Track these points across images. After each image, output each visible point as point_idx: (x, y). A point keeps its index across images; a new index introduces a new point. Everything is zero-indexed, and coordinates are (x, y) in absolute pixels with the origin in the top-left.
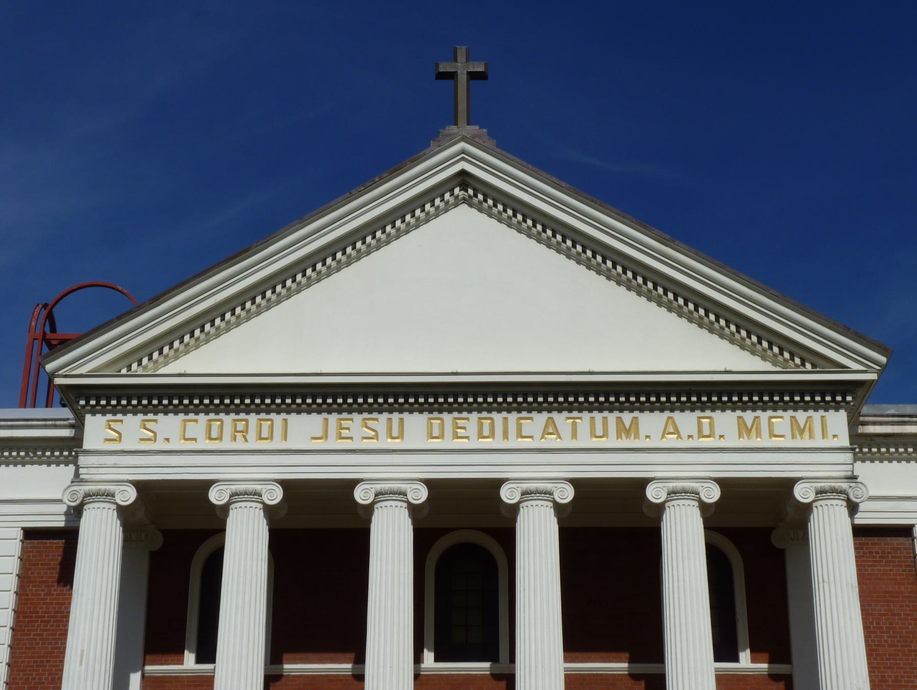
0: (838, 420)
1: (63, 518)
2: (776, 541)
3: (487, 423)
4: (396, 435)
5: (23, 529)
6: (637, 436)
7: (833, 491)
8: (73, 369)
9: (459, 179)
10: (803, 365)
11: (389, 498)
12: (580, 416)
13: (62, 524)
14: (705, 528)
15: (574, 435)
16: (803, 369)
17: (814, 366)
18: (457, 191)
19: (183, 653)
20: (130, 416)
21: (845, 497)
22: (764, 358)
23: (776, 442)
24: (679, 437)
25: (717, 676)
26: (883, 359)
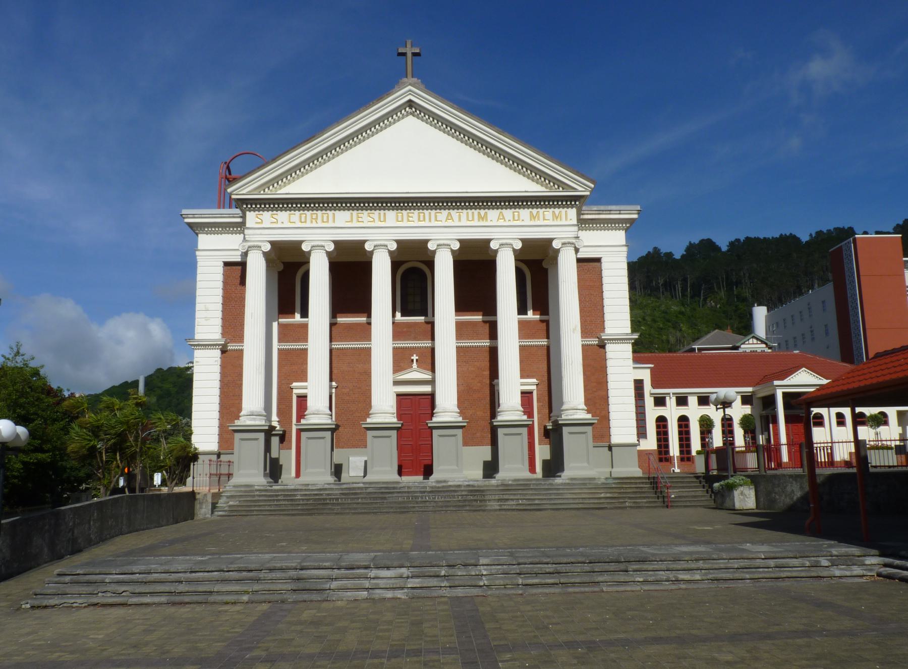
0: (572, 213)
1: (240, 257)
2: (545, 265)
3: (325, 216)
5: (223, 262)
7: (569, 243)
8: (240, 191)
9: (408, 104)
10: (559, 188)
13: (240, 260)
14: (515, 260)
15: (460, 220)
16: (558, 190)
17: (563, 189)
18: (407, 109)
19: (295, 314)
20: (266, 212)
22: (542, 185)
23: (546, 223)
24: (505, 220)
25: (518, 321)
26: (592, 186)
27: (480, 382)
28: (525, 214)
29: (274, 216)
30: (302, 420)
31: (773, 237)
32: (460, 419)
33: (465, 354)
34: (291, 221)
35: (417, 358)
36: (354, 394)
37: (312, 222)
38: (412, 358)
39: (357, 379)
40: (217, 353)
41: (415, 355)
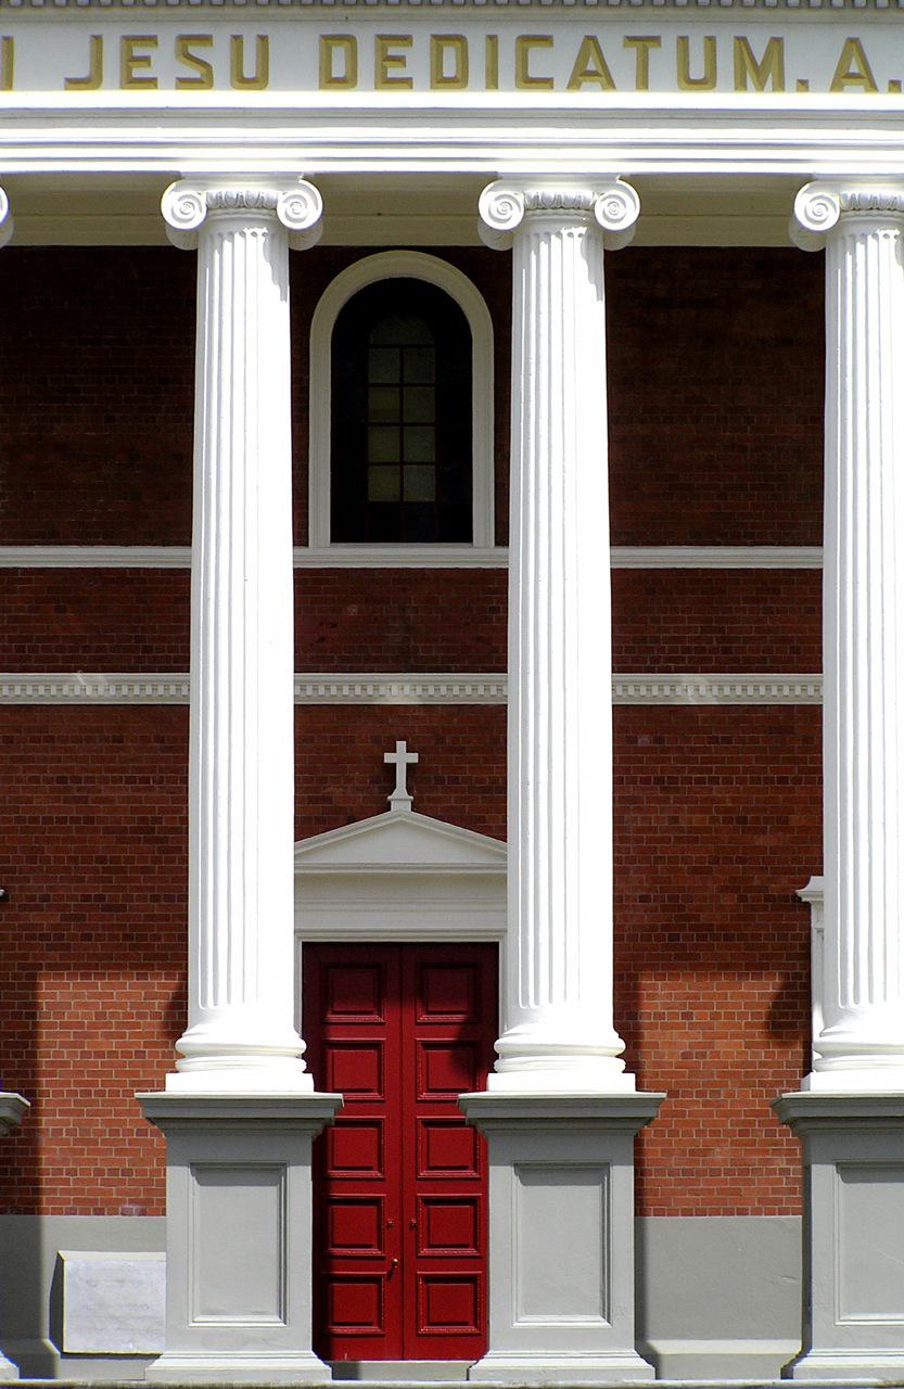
4: (701, 76)
6: (780, 86)
11: (870, 218)
12: (656, 34)
21: (214, 215)
27: (735, 890)
29: (194, 50)
30: (170, 1077)
31: (566, 198)
32: (625, 1085)
33: (659, 740)
34: (532, 74)
35: (414, 758)
36: (87, 937)
38: (388, 758)
39: (102, 860)
41: (401, 745)
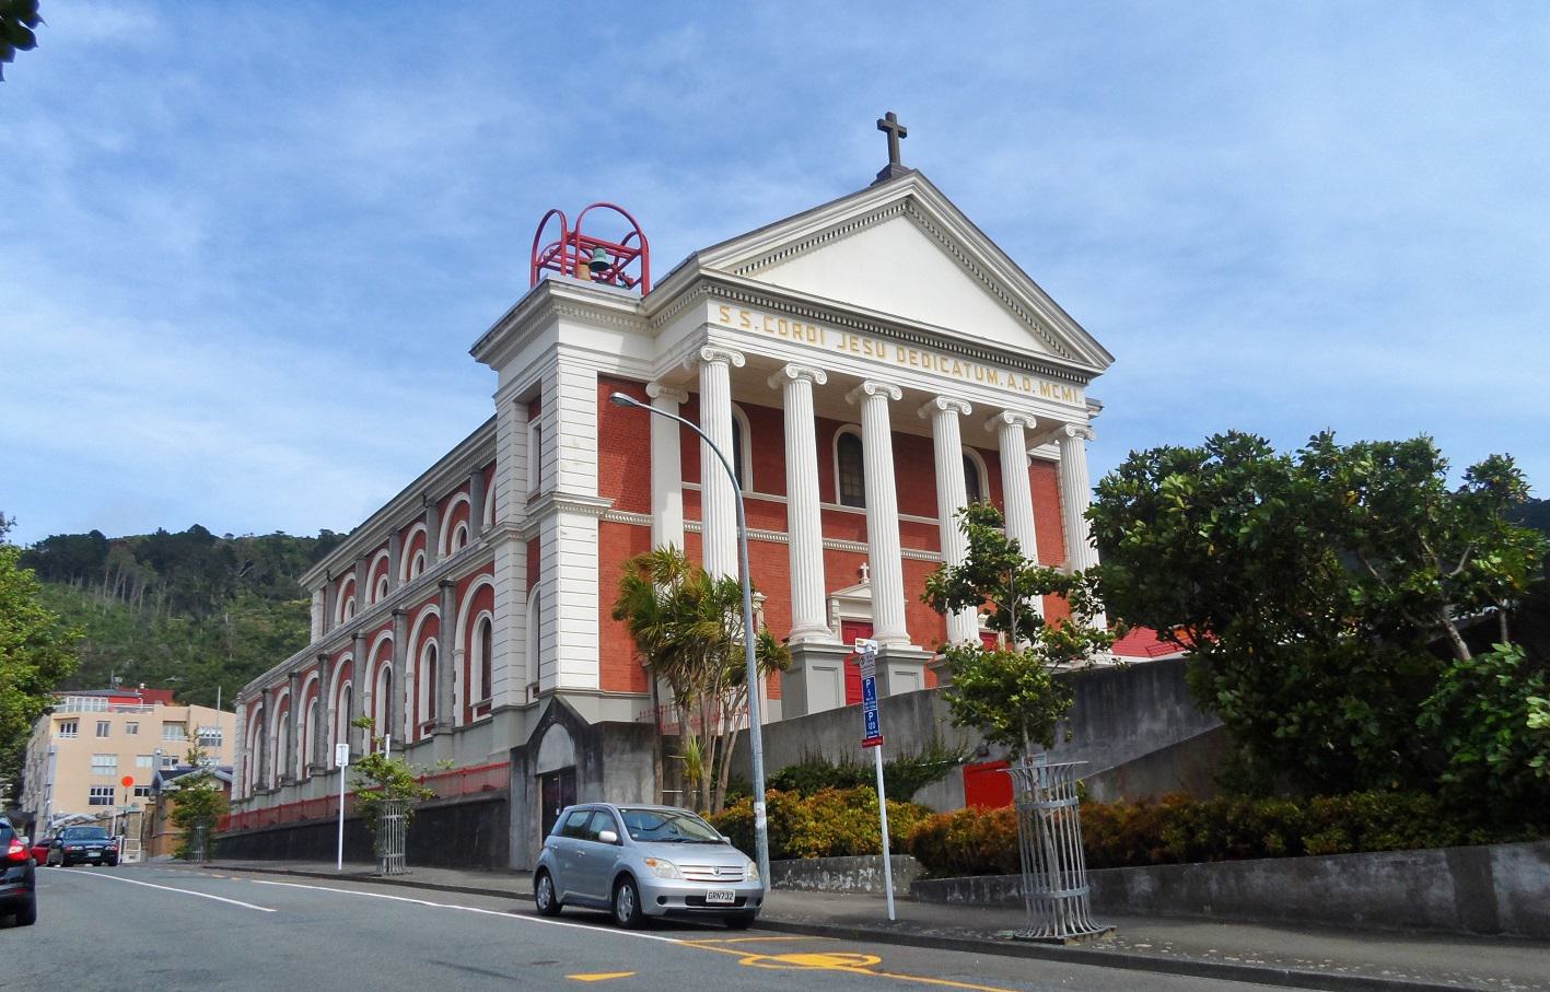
28: (1035, 384)
37: (794, 336)
40: (593, 523)
